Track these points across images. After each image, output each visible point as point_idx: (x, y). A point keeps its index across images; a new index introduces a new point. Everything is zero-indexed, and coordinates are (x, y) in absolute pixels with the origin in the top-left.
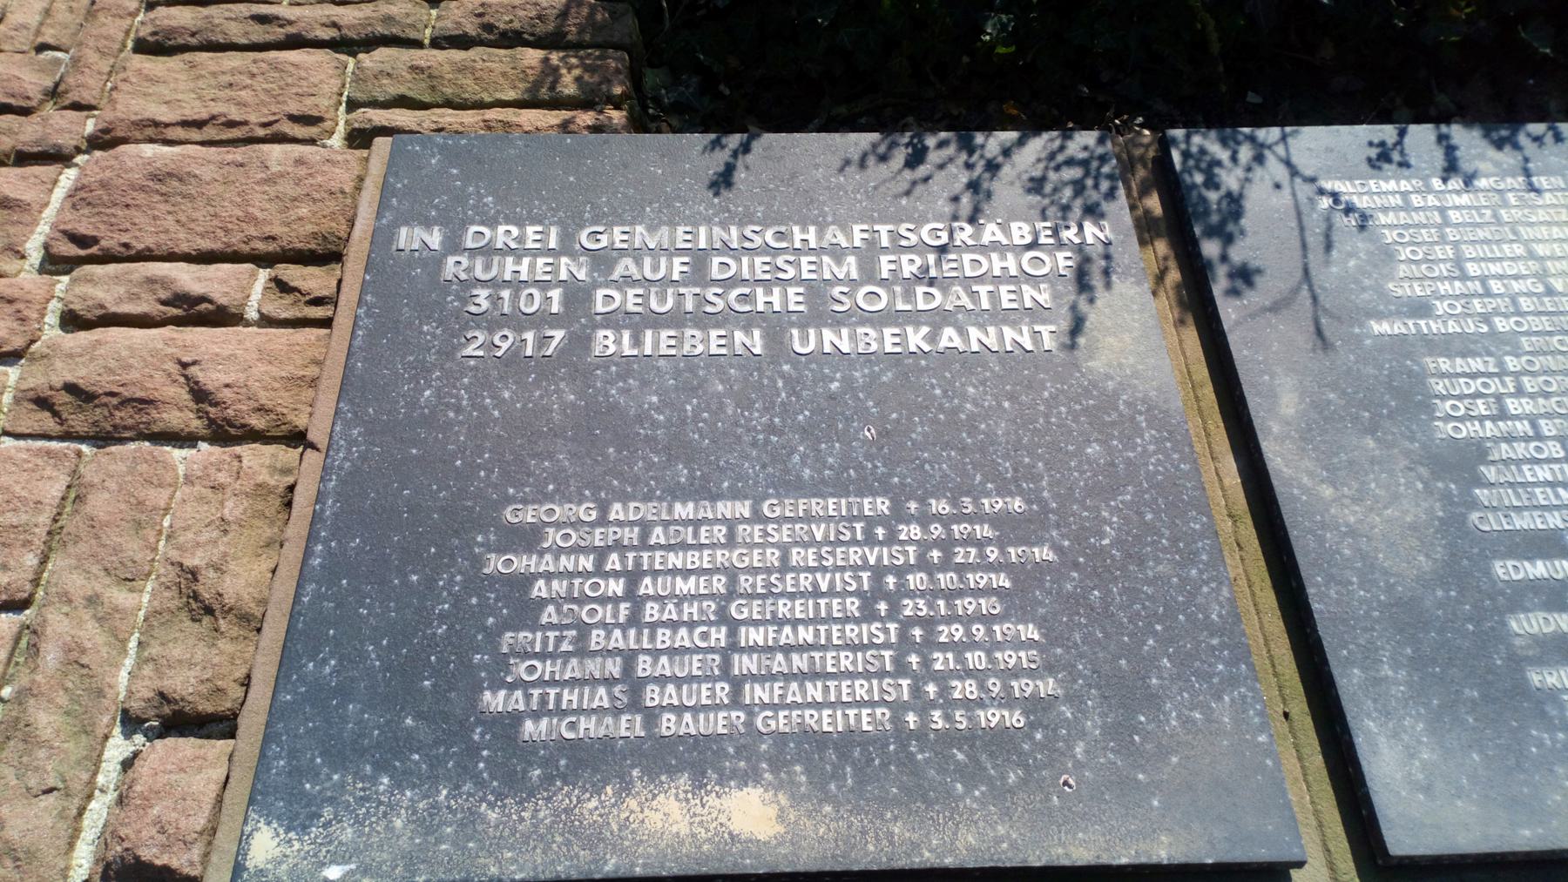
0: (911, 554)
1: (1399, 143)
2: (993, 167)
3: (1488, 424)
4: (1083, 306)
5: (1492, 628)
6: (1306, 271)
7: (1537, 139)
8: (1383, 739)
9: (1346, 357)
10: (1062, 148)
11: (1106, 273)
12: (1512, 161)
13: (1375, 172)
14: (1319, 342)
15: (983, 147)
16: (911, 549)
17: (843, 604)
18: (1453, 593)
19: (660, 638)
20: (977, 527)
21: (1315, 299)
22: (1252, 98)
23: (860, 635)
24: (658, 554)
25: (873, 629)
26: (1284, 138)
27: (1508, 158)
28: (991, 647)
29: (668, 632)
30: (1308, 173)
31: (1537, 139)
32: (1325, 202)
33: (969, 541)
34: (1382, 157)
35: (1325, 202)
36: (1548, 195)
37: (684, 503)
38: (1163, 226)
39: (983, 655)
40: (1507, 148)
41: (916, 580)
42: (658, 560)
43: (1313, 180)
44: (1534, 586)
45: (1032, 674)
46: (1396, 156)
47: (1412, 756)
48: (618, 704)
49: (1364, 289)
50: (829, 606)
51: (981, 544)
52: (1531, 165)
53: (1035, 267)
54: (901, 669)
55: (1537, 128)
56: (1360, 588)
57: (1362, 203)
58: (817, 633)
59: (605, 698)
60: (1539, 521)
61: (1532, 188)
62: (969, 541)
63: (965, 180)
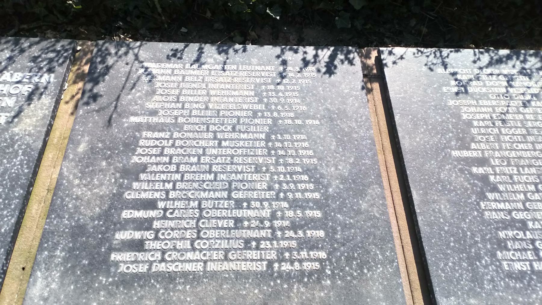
1: (183, 50)
2: (22, 51)
3: (481, 122)
4: (25, 107)
5: (108, 237)
6: (119, 97)
7: (236, 51)
8: (40, 280)
9: (115, 130)
10: (54, 45)
11: (41, 94)
12: (221, 59)
13: (168, 60)
14: (108, 124)
15: (23, 43)
18: (101, 223)
21: (116, 107)
22: (184, 30)
24: (224, 149)
26: (140, 46)
27: (221, 58)
30: (142, 59)
31: (236, 51)
32: (142, 71)
34: (175, 54)
35: (142, 71)
36: (227, 72)
38: (512, 54)
40: (223, 54)
42: (224, 151)
43: (142, 62)
44: (134, 220)
45: (312, 191)
46: (179, 55)
47: (47, 286)
49: (137, 105)
52: (228, 61)
54: (270, 188)
55: (238, 46)
56: (67, 220)
57: (154, 72)
60: (470, 154)
61: (224, 70)
63: (8, 56)
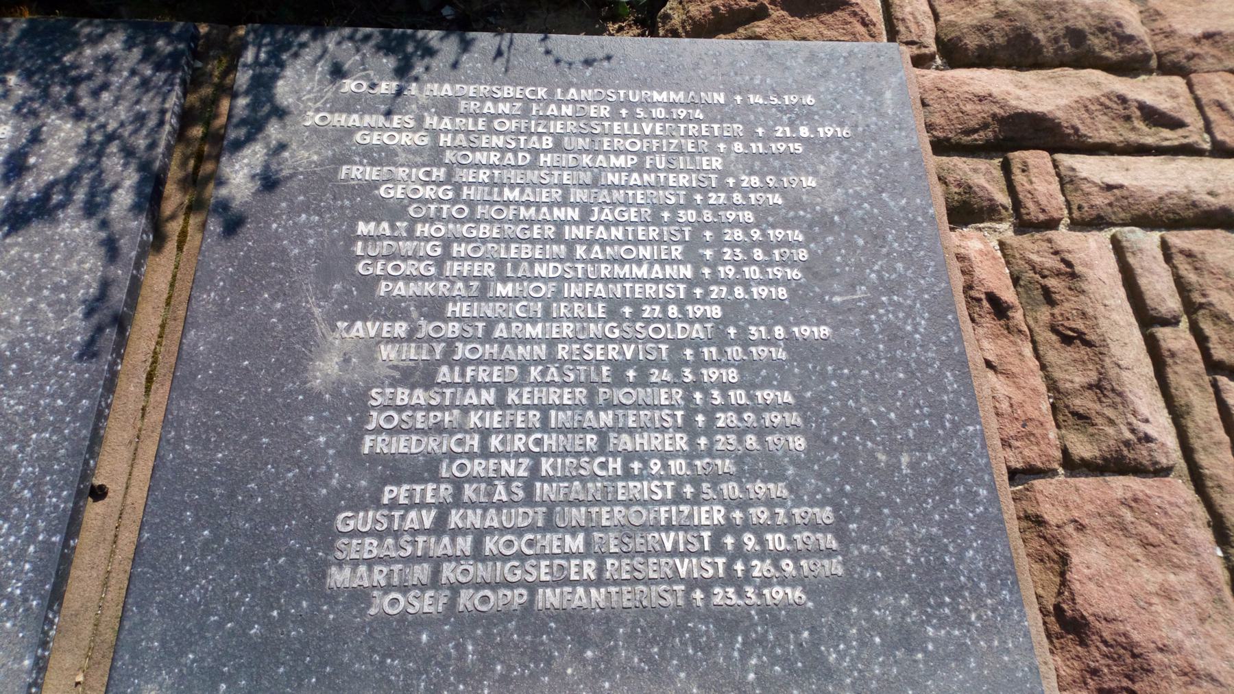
0: (687, 234)
16: (687, 229)
17: (638, 212)
19: (544, 142)
20: (773, 290)
23: (657, 292)
25: (667, 288)
28: (789, 529)
29: (529, 246)
33: (736, 224)
37: (367, 222)
39: (740, 350)
41: (710, 352)
48: (515, 498)
50: (632, 289)
51: (746, 227)
53: (499, 214)
58: (626, 232)
59: (503, 492)
62: (736, 224)
